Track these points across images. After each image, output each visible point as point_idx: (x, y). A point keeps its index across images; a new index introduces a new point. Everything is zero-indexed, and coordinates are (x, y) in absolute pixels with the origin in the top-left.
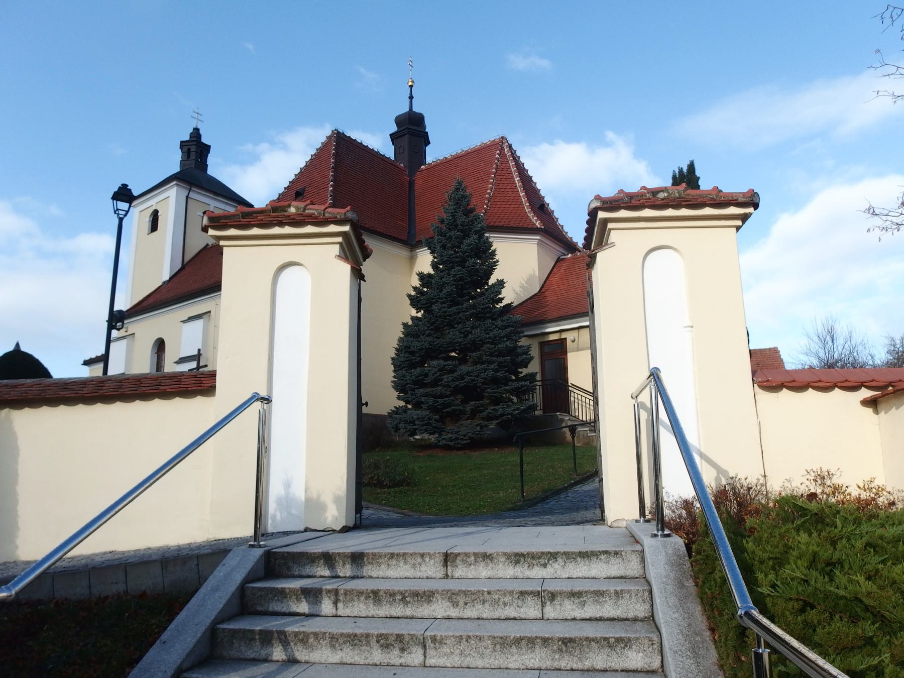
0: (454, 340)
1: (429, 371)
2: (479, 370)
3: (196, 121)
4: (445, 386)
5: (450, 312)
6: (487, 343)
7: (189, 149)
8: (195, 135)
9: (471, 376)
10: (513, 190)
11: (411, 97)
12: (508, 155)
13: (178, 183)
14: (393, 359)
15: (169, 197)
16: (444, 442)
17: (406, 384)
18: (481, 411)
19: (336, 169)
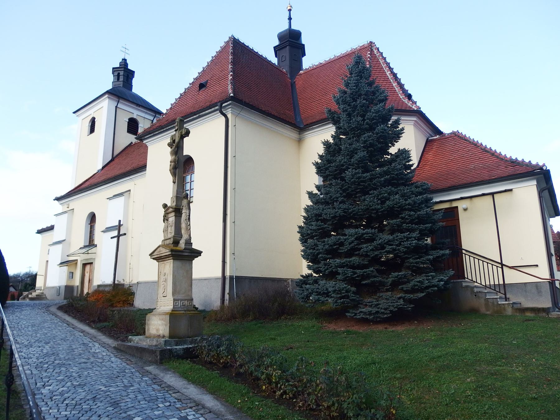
0: (371, 207)
1: (345, 240)
2: (400, 239)
3: (124, 53)
4: (362, 255)
5: (364, 178)
6: (406, 210)
7: (119, 74)
8: (123, 63)
9: (392, 245)
10: (386, 81)
11: (290, 19)
12: (377, 55)
13: (109, 96)
14: (300, 227)
15: (103, 107)
16: (362, 315)
17: (318, 254)
18: (404, 283)
19: (234, 63)
